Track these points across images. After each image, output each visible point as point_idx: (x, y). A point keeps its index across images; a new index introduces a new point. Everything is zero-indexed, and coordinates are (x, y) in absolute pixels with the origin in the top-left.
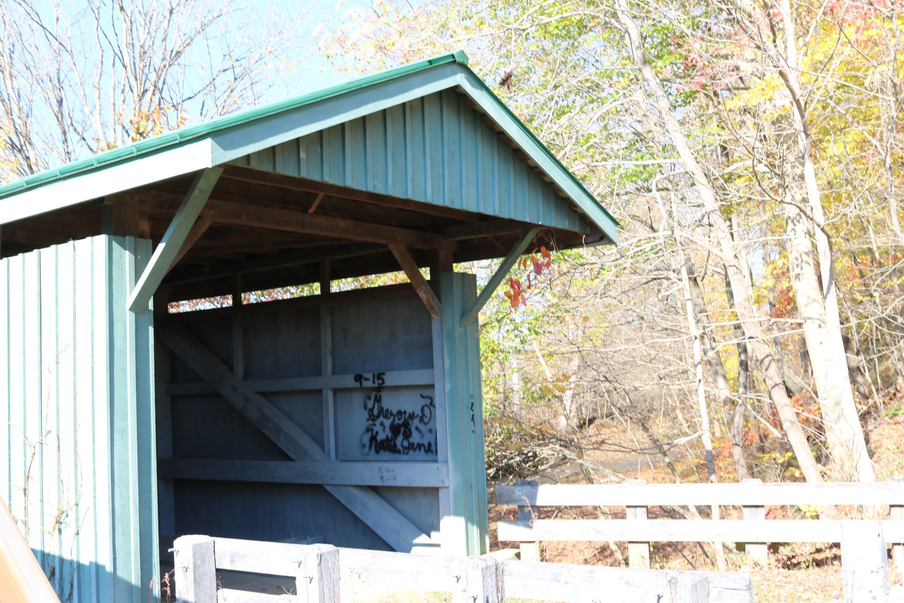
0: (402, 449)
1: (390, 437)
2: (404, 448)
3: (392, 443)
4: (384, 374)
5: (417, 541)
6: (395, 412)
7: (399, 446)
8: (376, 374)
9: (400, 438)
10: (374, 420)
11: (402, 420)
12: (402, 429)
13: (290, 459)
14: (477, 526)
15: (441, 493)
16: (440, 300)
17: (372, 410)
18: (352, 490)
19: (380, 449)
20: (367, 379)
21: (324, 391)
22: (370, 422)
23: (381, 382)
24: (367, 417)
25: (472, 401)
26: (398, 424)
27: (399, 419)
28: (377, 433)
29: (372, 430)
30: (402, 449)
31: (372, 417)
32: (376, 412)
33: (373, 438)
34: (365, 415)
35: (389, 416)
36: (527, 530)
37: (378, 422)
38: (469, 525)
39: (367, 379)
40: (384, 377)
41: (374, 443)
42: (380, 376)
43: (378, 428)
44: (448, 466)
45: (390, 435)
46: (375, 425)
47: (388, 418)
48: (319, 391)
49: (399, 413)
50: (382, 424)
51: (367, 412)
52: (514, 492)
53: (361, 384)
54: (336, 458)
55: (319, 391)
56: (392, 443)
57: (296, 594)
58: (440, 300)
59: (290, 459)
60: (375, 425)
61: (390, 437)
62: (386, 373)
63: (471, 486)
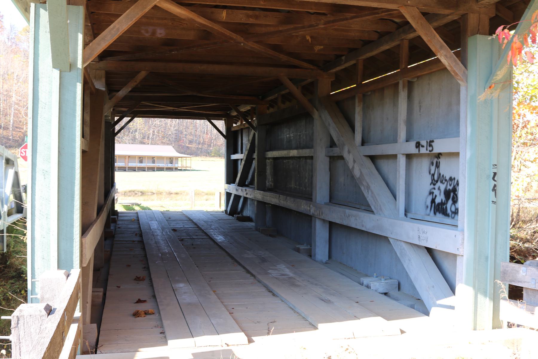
0: (450, 213)
1: (443, 201)
2: (453, 212)
3: (445, 207)
4: (433, 141)
5: (439, 302)
6: (448, 178)
7: (449, 211)
8: (428, 141)
9: (450, 202)
10: (434, 185)
11: (452, 186)
12: (452, 194)
13: (372, 212)
14: (490, 298)
15: (459, 259)
16: (465, 66)
17: (433, 175)
18: (403, 244)
19: (437, 211)
20: (423, 146)
21: (398, 156)
22: (432, 186)
23: (431, 149)
24: (430, 181)
25: (495, 171)
26: (449, 189)
27: (450, 185)
28: (436, 196)
29: (433, 193)
30: (450, 213)
31: (434, 182)
32: (436, 177)
33: (433, 201)
34: (429, 179)
35: (444, 181)
36: (528, 314)
37: (436, 187)
38: (480, 297)
39: (423, 146)
40: (433, 144)
41: (433, 205)
42: (430, 143)
43: (436, 192)
44: (464, 235)
45: (444, 199)
46: (434, 189)
47: (443, 183)
48: (395, 157)
49: (451, 179)
50: (439, 189)
51: (430, 176)
52: (518, 272)
53: (419, 151)
54: (406, 215)
55: (395, 157)
56: (445, 207)
57: (493, 329)
58: (465, 66)
59: (372, 212)
60: (434, 189)
61: (443, 201)
62: (435, 140)
63: (487, 258)
